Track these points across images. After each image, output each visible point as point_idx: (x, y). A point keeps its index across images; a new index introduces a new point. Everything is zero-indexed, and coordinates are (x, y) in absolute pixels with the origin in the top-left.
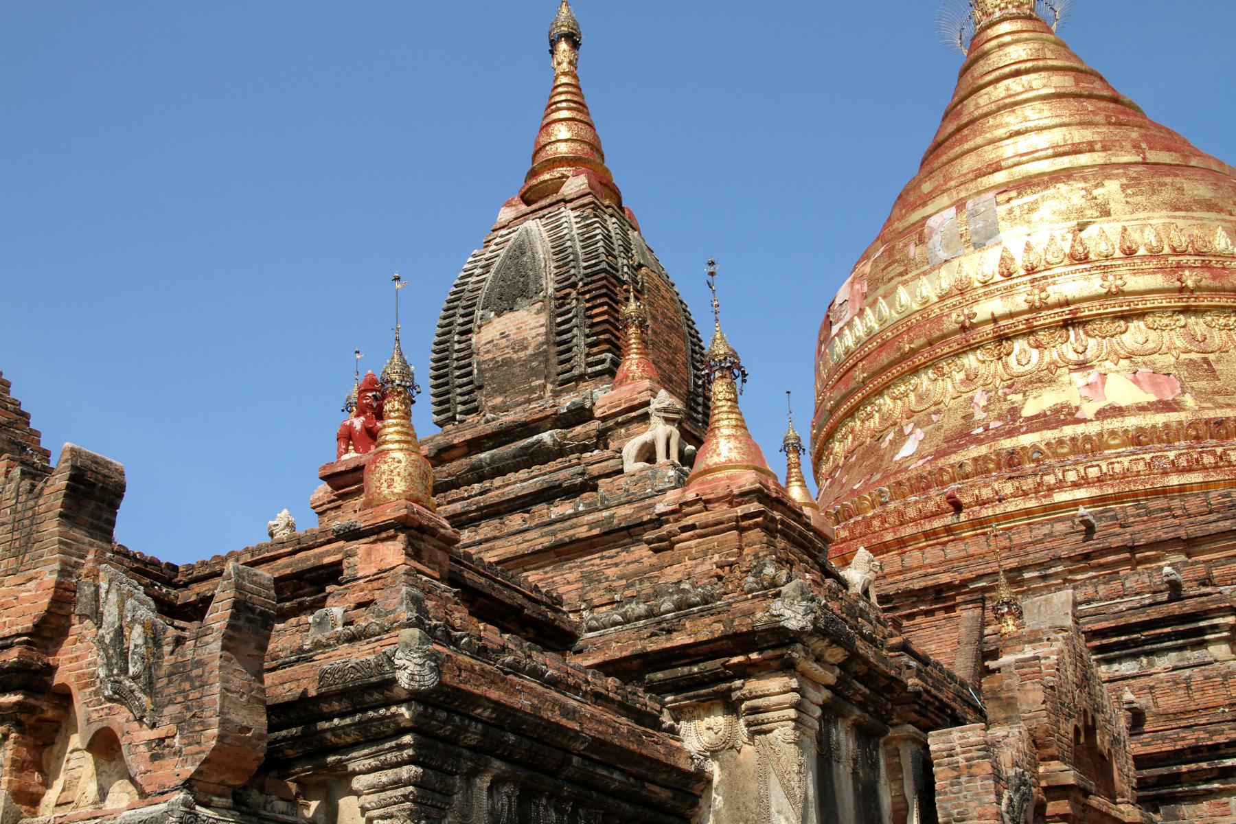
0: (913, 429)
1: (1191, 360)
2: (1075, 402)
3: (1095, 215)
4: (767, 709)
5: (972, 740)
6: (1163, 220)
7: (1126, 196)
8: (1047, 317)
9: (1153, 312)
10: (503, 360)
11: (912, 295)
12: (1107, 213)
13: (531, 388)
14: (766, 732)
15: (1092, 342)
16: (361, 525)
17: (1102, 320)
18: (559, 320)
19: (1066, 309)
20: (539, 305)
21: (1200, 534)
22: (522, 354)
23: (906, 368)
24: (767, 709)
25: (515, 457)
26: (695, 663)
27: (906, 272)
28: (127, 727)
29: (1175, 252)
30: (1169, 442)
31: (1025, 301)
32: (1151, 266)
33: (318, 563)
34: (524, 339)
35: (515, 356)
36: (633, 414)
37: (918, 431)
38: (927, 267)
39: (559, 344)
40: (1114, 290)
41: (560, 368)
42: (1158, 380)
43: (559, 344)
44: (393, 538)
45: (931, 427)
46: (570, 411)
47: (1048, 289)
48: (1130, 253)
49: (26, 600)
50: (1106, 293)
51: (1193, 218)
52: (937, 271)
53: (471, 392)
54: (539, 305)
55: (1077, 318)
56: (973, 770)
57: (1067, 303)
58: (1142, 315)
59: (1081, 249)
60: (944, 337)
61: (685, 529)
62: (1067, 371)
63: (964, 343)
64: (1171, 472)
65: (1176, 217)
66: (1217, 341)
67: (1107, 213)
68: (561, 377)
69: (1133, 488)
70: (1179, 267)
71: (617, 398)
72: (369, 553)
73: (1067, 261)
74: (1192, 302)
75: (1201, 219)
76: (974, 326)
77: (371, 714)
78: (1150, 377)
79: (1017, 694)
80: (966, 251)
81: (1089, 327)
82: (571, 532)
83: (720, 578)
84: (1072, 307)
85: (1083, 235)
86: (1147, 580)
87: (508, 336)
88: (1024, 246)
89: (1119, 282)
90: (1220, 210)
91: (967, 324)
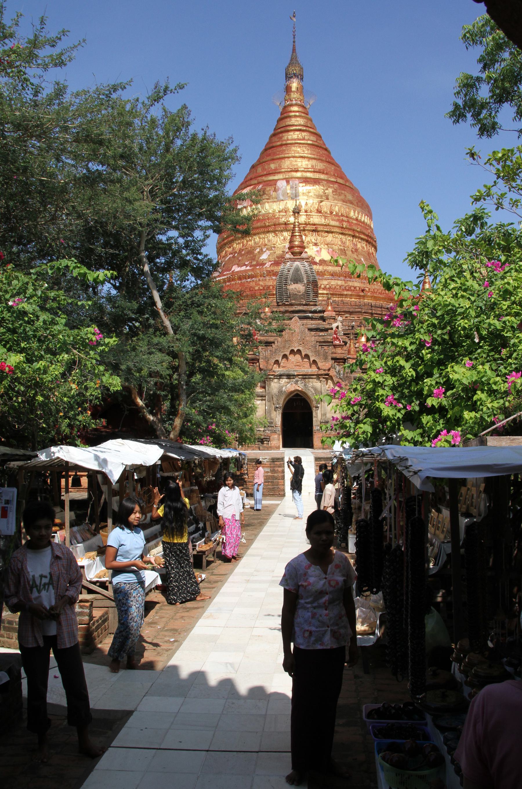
2: (313, 256)
8: (309, 227)
11: (270, 207)
12: (328, 199)
15: (319, 238)
27: (269, 199)
29: (342, 215)
48: (331, 213)
57: (314, 225)
58: (332, 232)
67: (328, 199)
70: (343, 221)
74: (344, 232)
76: (288, 224)
85: (321, 204)
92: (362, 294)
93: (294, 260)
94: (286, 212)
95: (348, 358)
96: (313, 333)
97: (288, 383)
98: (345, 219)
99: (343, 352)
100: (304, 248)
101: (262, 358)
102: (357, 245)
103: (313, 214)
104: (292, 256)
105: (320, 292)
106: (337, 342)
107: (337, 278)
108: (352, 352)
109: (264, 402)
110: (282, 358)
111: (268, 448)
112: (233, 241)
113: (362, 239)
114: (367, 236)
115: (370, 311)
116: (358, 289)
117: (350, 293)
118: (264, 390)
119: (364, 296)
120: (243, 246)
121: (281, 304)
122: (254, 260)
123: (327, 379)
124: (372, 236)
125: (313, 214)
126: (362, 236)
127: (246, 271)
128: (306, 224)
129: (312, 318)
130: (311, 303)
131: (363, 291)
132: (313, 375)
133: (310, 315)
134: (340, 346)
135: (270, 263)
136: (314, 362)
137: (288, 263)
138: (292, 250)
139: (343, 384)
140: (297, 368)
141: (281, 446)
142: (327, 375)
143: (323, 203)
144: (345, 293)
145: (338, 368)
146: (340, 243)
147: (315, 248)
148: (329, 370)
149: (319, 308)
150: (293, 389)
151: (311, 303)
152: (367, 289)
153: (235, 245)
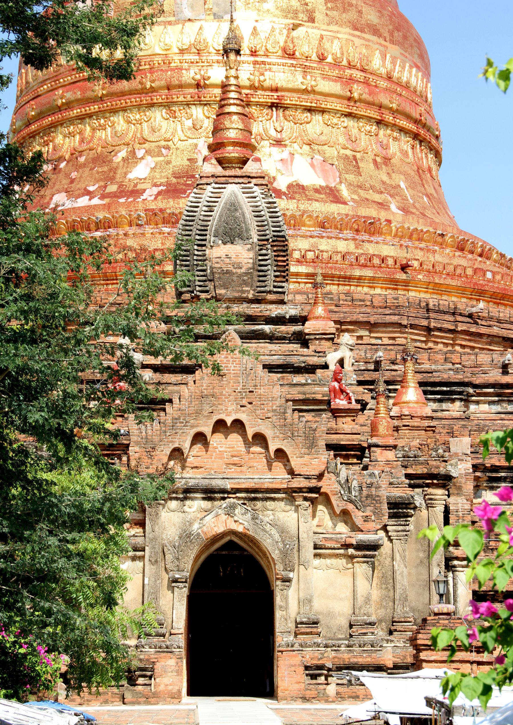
0: (144, 156)
1: (346, 155)
2: (272, 174)
3: (304, 20)
4: (435, 500)
5: (466, 508)
6: (346, 36)
7: (327, 9)
8: (261, 97)
9: (329, 112)
10: (227, 270)
12: (312, 20)
13: (242, 290)
14: (433, 507)
15: (287, 125)
16: (380, 444)
17: (296, 109)
18: (260, 258)
19: (275, 94)
20: (249, 246)
21: (380, 321)
22: (239, 271)
23: (145, 102)
24: (435, 500)
25: (247, 333)
26: (412, 480)
28: (353, 510)
29: (350, 66)
30: (341, 230)
31: (248, 79)
32: (334, 74)
33: (338, 443)
34: (240, 263)
35: (234, 271)
36: (324, 336)
37: (148, 158)
38: (172, 19)
39: (259, 271)
40: (309, 89)
41: (259, 284)
42: (326, 168)
43: (259, 271)
44: (391, 450)
45: (162, 159)
46: (277, 317)
47: (267, 73)
48: (322, 58)
49: (314, 464)
50: (304, 90)
51: (364, 38)
52: (180, 26)
53: (205, 281)
54: (249, 246)
55: (281, 104)
56: (464, 518)
57: (276, 90)
58: (323, 111)
59: (291, 46)
60: (181, 86)
61: (404, 426)
62: (269, 145)
63: (196, 98)
64: (355, 265)
65: (354, 36)
66: (363, 144)
67: (312, 20)
68: (259, 289)
69: (334, 273)
70: (351, 80)
71: (318, 326)
72: (381, 453)
73: (280, 53)
74: (354, 110)
75: (368, 40)
76: (206, 86)
77: (400, 510)
78: (321, 164)
79: (463, 485)
80: (208, 17)
81: (287, 113)
82: (313, 396)
83: (419, 449)
84: (279, 94)
85: (294, 34)
86: (363, 354)
87: (230, 258)
88: (251, 29)
89: (313, 83)
90: (380, 36)
91: (202, 83)
92: (402, 276)
93: (226, 180)
94: (199, 52)
95: (370, 446)
96: (275, 376)
97: (208, 511)
98: (358, 75)
99: (357, 428)
100: (253, 148)
101: (137, 443)
102: (386, 147)
103: (272, 59)
104: (219, 170)
105: (293, 269)
106: (341, 403)
107: (334, 232)
108: (382, 429)
109: (139, 564)
110: (193, 444)
111: (148, 699)
112: (54, 126)
113: (402, 130)
114: (416, 122)
115: (425, 323)
116: (390, 262)
117: (368, 273)
118: (141, 530)
119: (406, 284)
120: (82, 141)
121: (187, 296)
122: (112, 179)
123: (313, 501)
124: (429, 122)
125: (272, 59)
126: (404, 123)
127: (88, 209)
128: (252, 87)
129: (271, 338)
130: (270, 297)
131: (404, 268)
132: (277, 491)
133: (267, 328)
134: (348, 412)
135: (155, 190)
136: (280, 453)
137: (209, 188)
138: (219, 153)
139: (358, 516)
140: (233, 471)
141: (184, 691)
142: (316, 490)
143: (300, 32)
144: (357, 272)
145: (344, 472)
146: (342, 140)
147: (277, 153)
148: (320, 476)
149: (290, 311)
150: (220, 529)
151: (270, 297)
152: (416, 264)
153: (59, 139)
